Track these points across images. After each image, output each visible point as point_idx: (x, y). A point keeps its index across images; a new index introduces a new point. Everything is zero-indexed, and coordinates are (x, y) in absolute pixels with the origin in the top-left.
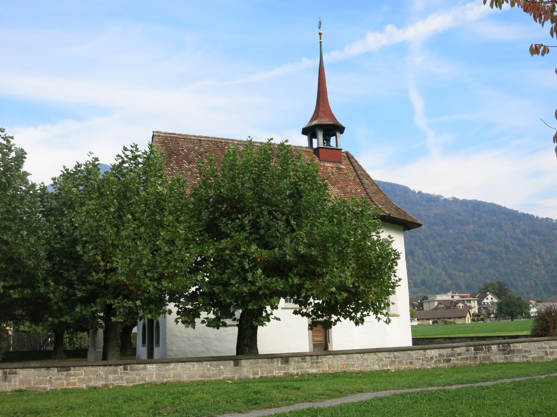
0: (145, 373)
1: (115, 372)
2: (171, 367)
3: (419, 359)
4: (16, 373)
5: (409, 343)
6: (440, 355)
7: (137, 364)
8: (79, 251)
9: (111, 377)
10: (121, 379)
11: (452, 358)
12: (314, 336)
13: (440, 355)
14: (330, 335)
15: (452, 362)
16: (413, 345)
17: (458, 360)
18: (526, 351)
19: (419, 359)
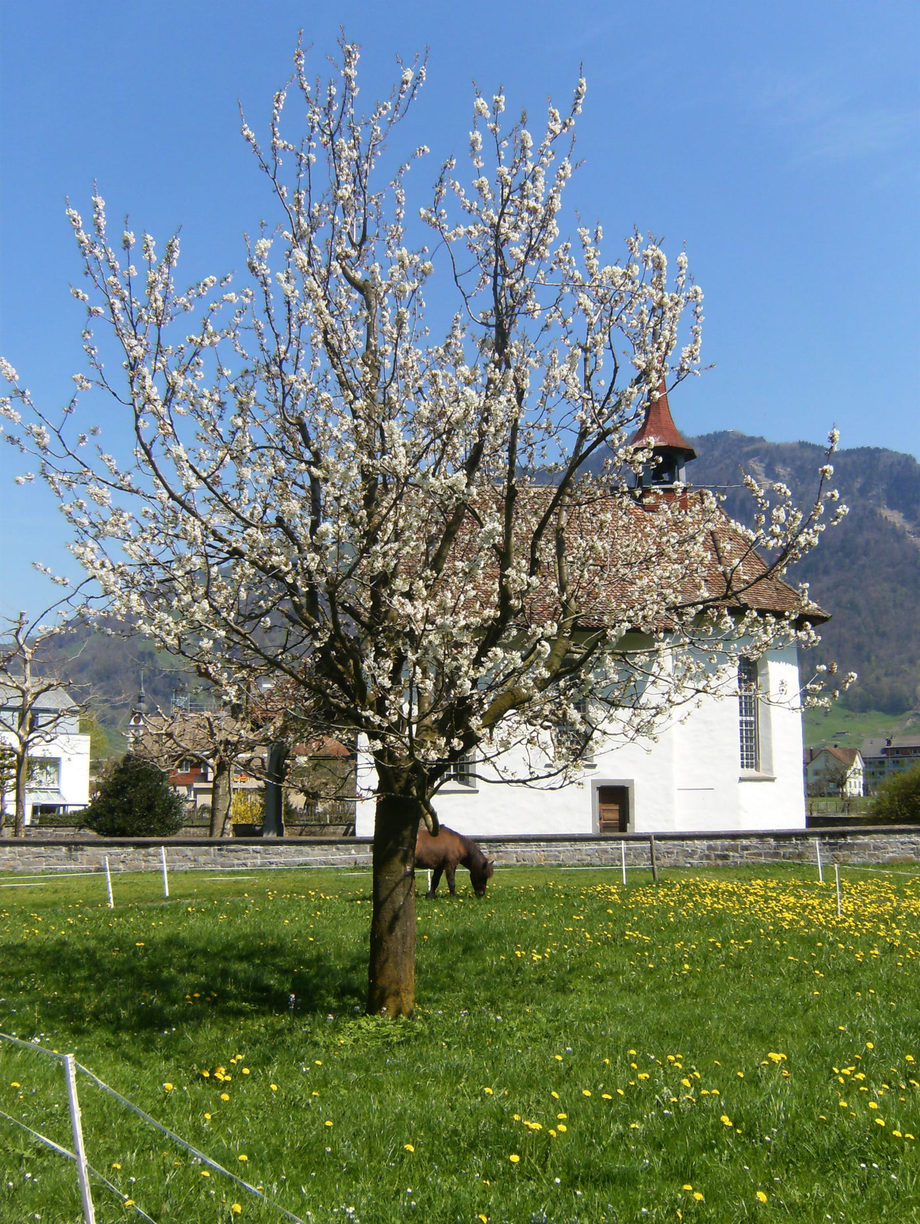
0: (246, 856)
1: (207, 853)
2: (57, 853)
3: (672, 853)
4: (82, 850)
5: (799, 823)
6: (710, 848)
7: (414, 849)
8: (245, 1020)
9: (202, 859)
10: (214, 862)
11: (731, 854)
12: (602, 811)
13: (710, 848)
14: (630, 810)
15: (731, 859)
16: (808, 825)
17: (742, 857)
18: (876, 848)
19: (672, 853)
